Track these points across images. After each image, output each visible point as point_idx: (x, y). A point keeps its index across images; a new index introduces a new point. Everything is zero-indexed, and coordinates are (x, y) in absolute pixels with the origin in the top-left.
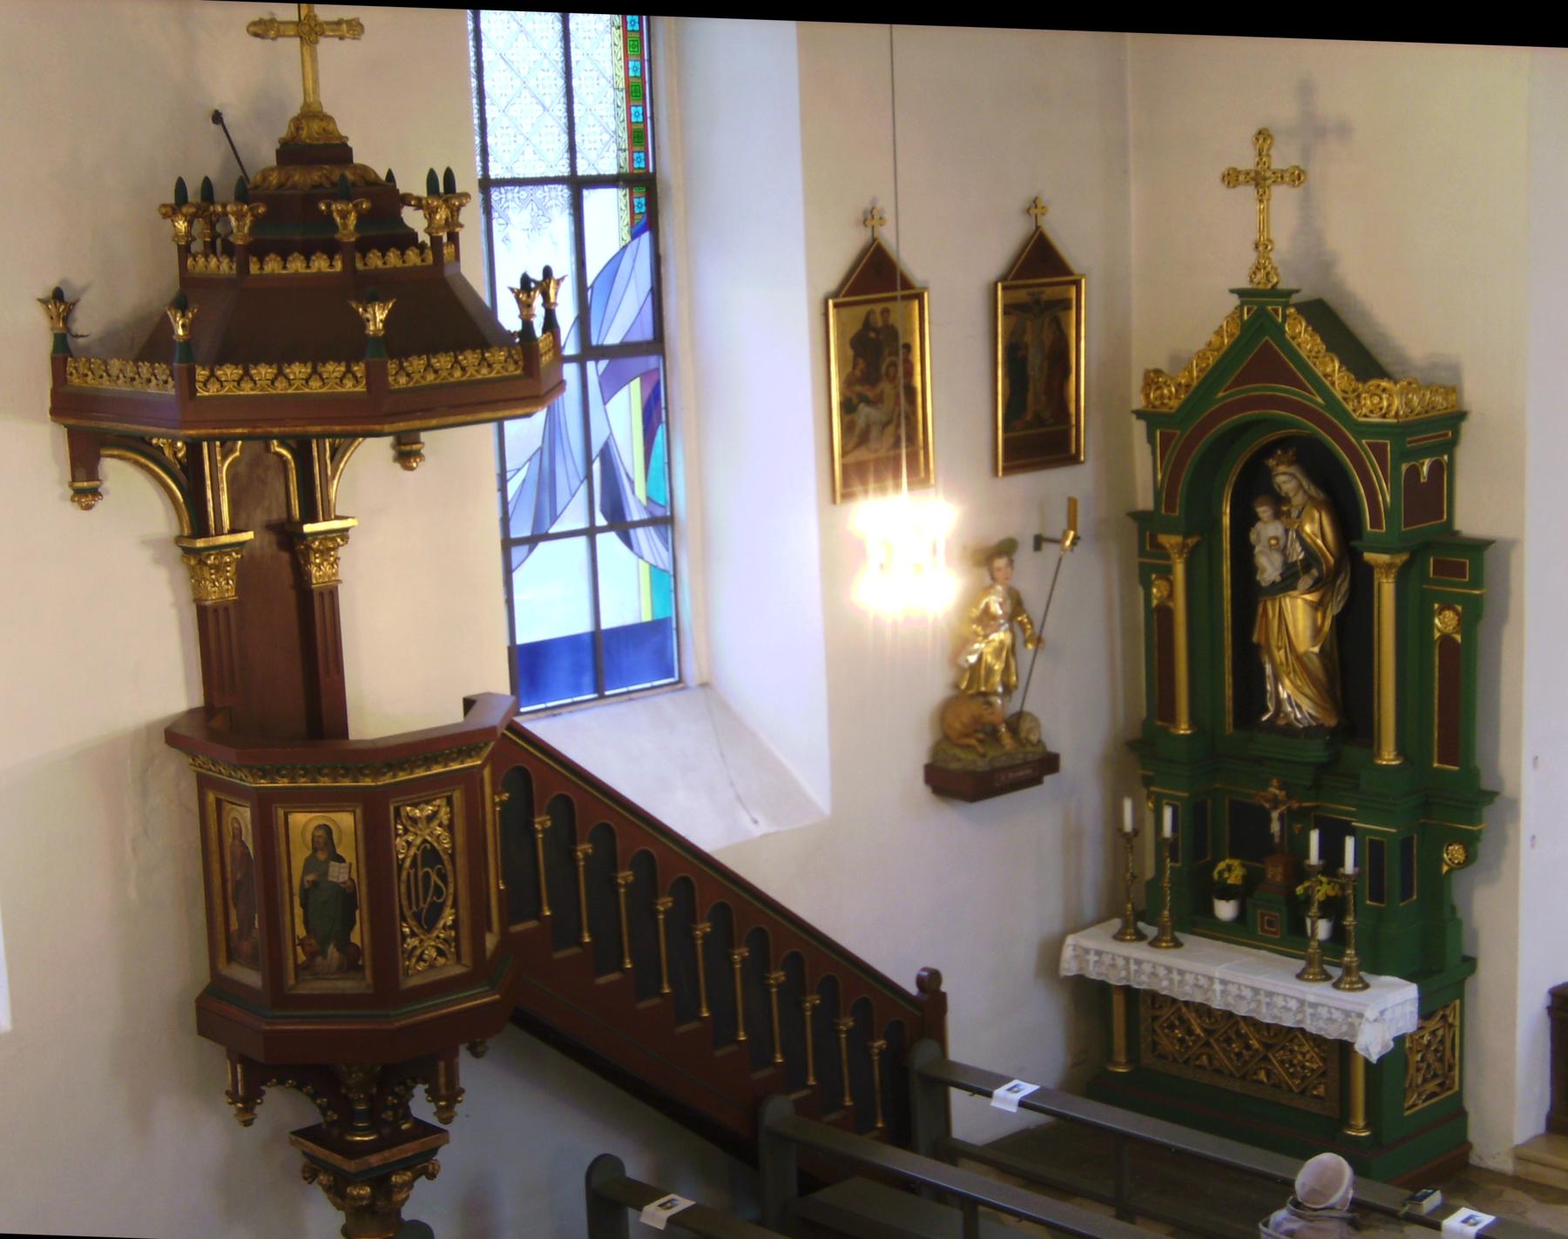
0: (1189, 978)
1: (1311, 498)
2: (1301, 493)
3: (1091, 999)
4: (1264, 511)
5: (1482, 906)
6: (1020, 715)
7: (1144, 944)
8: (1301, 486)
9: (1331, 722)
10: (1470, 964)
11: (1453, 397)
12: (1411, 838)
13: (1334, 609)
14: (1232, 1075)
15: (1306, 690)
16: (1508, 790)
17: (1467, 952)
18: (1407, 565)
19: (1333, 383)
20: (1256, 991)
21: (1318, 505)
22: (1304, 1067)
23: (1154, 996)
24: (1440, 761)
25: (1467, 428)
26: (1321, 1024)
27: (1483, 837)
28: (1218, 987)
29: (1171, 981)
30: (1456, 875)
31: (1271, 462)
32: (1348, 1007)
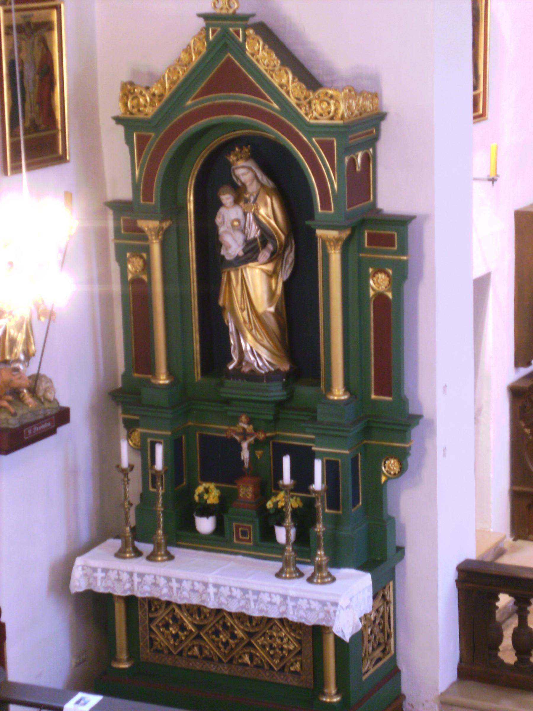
0: (187, 585)
1: (262, 186)
2: (255, 183)
3: (95, 610)
4: (227, 198)
5: (407, 504)
6: (37, 378)
7: (142, 560)
8: (256, 177)
9: (286, 367)
10: (400, 550)
11: (376, 101)
12: (357, 456)
13: (285, 275)
14: (220, 660)
15: (265, 342)
16: (426, 412)
17: (398, 544)
18: (349, 239)
19: (288, 93)
20: (245, 591)
21: (268, 191)
22: (282, 649)
23: (152, 603)
24: (376, 393)
25: (384, 125)
26: (301, 613)
27: (412, 452)
28: (212, 590)
29: (171, 588)
30: (389, 483)
31: (232, 158)
32: (324, 598)
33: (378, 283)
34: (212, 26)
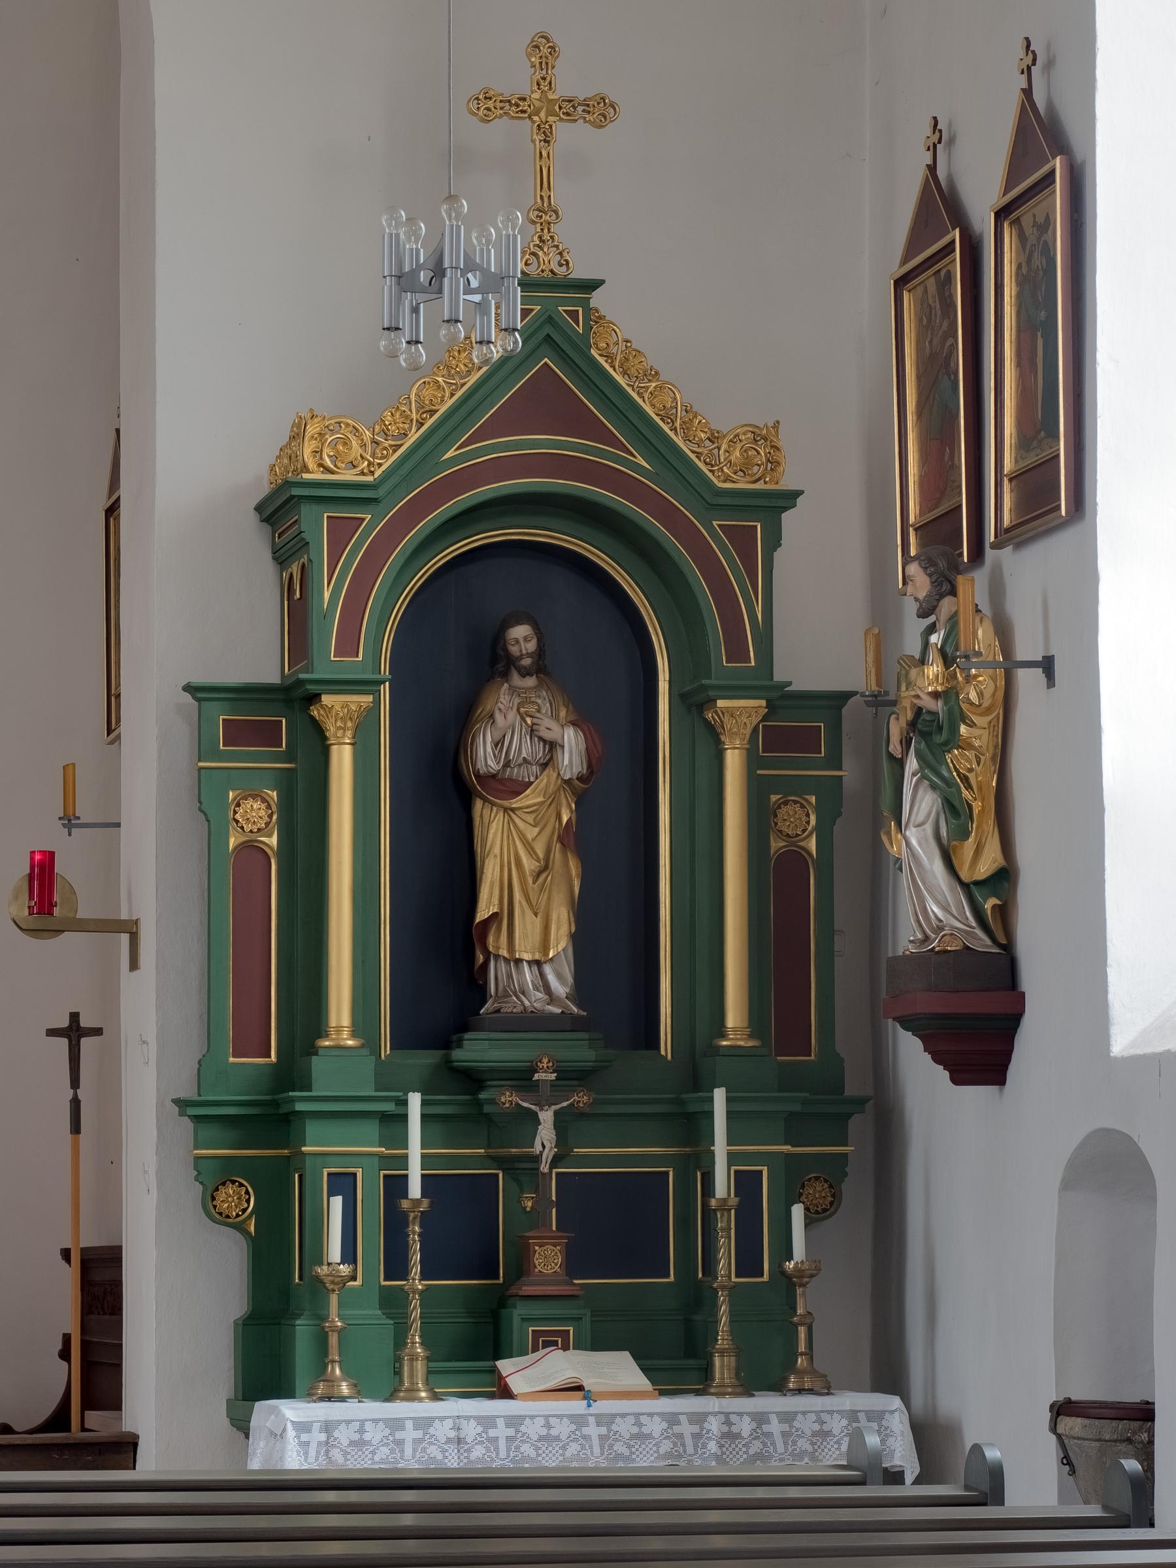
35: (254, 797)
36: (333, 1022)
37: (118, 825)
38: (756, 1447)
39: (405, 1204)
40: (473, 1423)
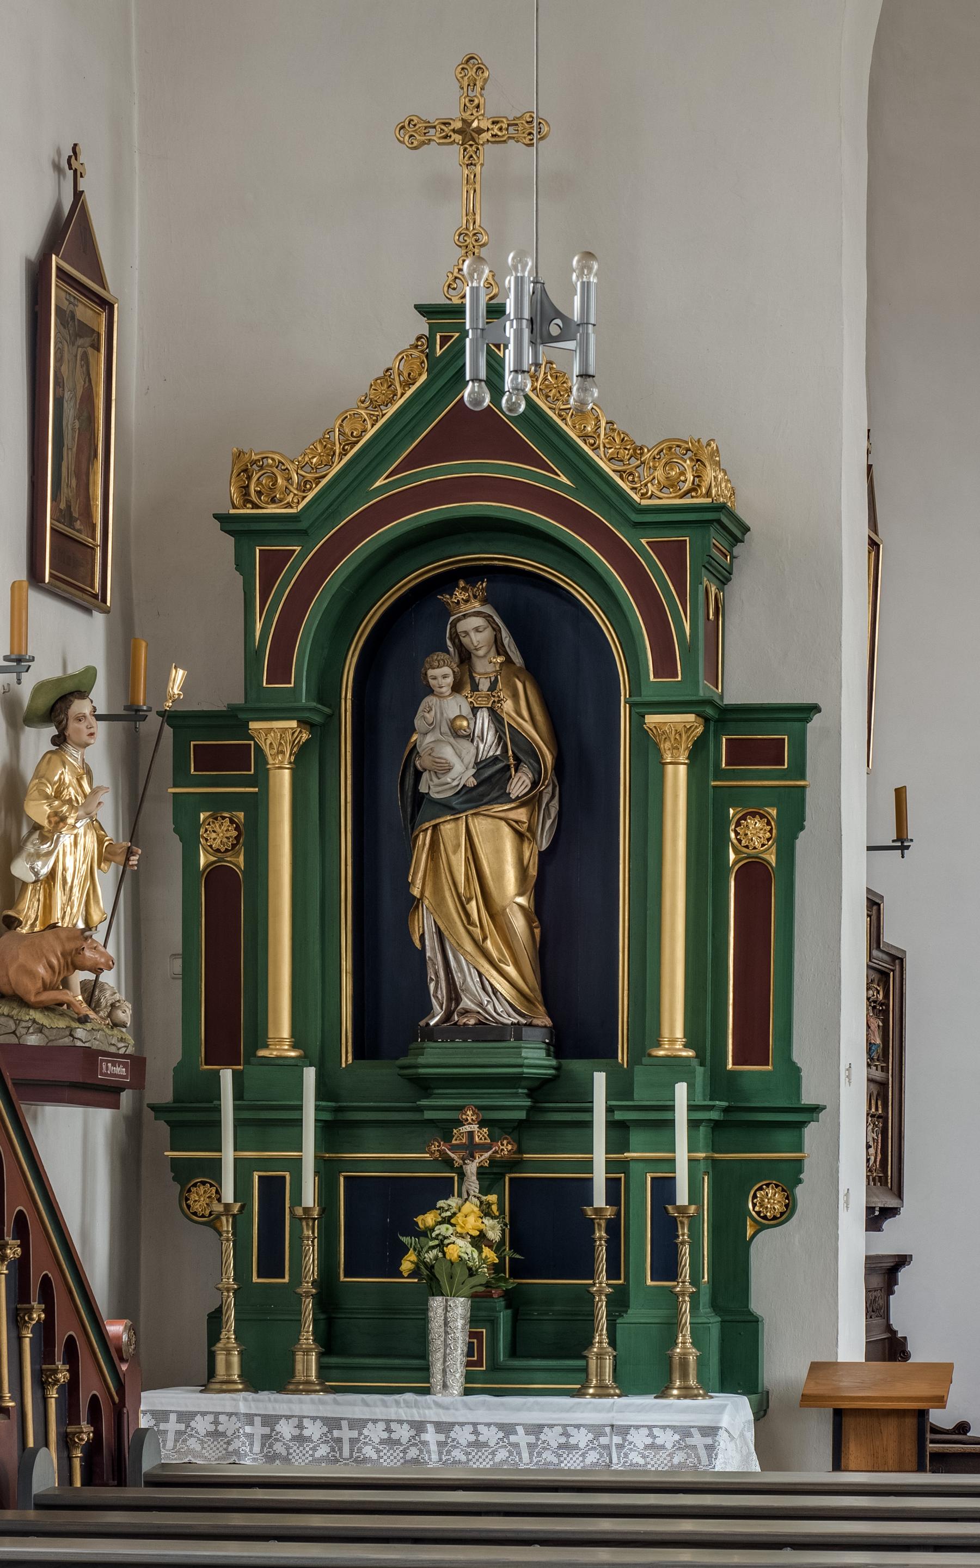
4: (441, 674)
33: (754, 835)
34: (441, 328)
35: (753, 815)
36: (666, 1032)
37: (869, 848)
38: (413, 1453)
39: (589, 1210)
40: (406, 1426)
